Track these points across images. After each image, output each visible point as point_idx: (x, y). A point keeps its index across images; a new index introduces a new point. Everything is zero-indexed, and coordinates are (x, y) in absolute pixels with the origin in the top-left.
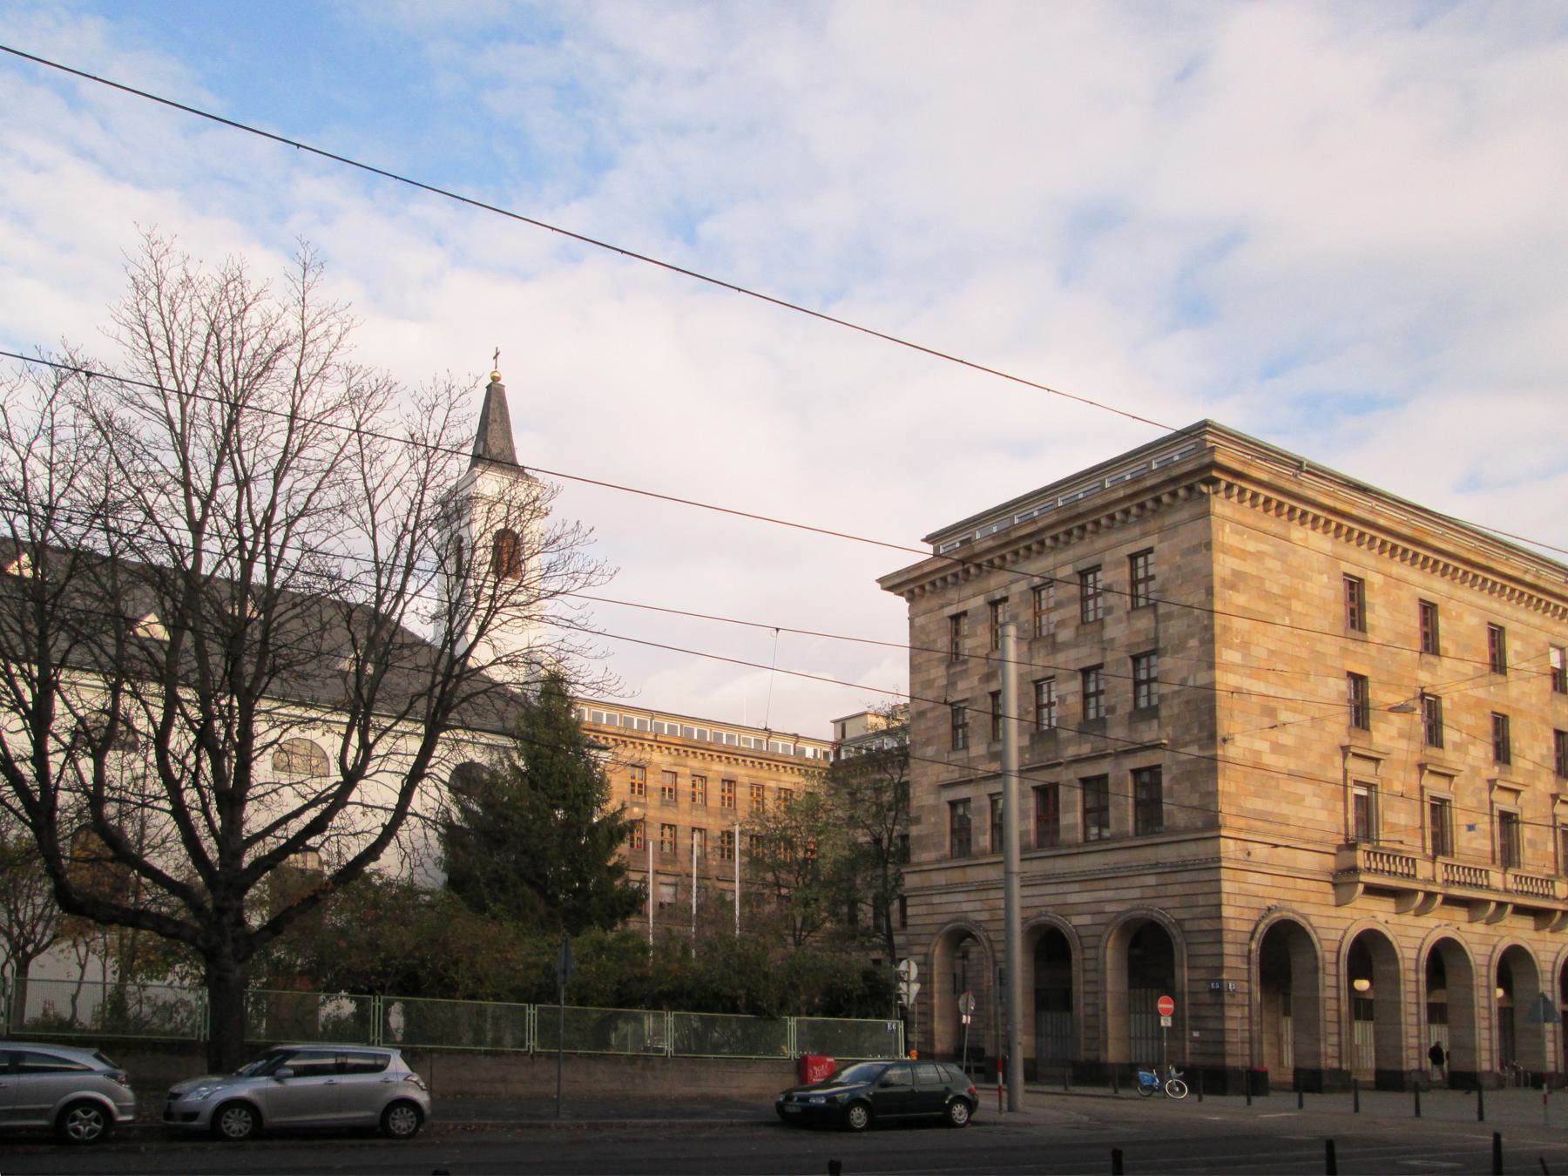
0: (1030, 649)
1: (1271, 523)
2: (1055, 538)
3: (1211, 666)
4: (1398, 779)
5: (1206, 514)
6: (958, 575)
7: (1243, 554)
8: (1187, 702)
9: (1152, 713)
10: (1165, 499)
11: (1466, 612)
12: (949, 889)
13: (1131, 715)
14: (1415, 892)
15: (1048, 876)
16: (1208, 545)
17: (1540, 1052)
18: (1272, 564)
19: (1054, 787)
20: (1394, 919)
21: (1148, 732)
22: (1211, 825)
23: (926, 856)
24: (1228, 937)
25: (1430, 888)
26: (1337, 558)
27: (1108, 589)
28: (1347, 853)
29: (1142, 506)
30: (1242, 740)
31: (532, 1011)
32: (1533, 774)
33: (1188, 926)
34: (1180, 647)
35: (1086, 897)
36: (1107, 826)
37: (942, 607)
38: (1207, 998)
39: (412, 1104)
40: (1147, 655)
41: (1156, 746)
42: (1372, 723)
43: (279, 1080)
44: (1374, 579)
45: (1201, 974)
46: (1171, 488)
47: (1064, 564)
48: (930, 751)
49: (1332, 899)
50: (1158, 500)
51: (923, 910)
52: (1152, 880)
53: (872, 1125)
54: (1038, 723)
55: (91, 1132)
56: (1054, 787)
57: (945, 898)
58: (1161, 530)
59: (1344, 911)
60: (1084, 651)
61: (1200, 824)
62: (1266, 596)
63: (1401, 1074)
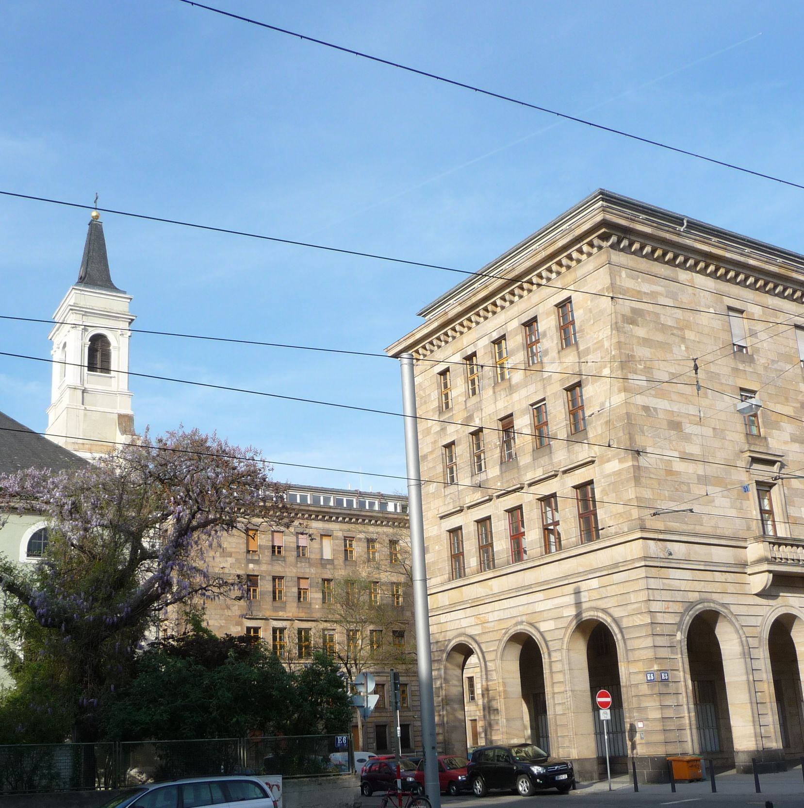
8: (608, 422)
35: (549, 604)
56: (520, 507)
60: (532, 388)
62: (664, 328)
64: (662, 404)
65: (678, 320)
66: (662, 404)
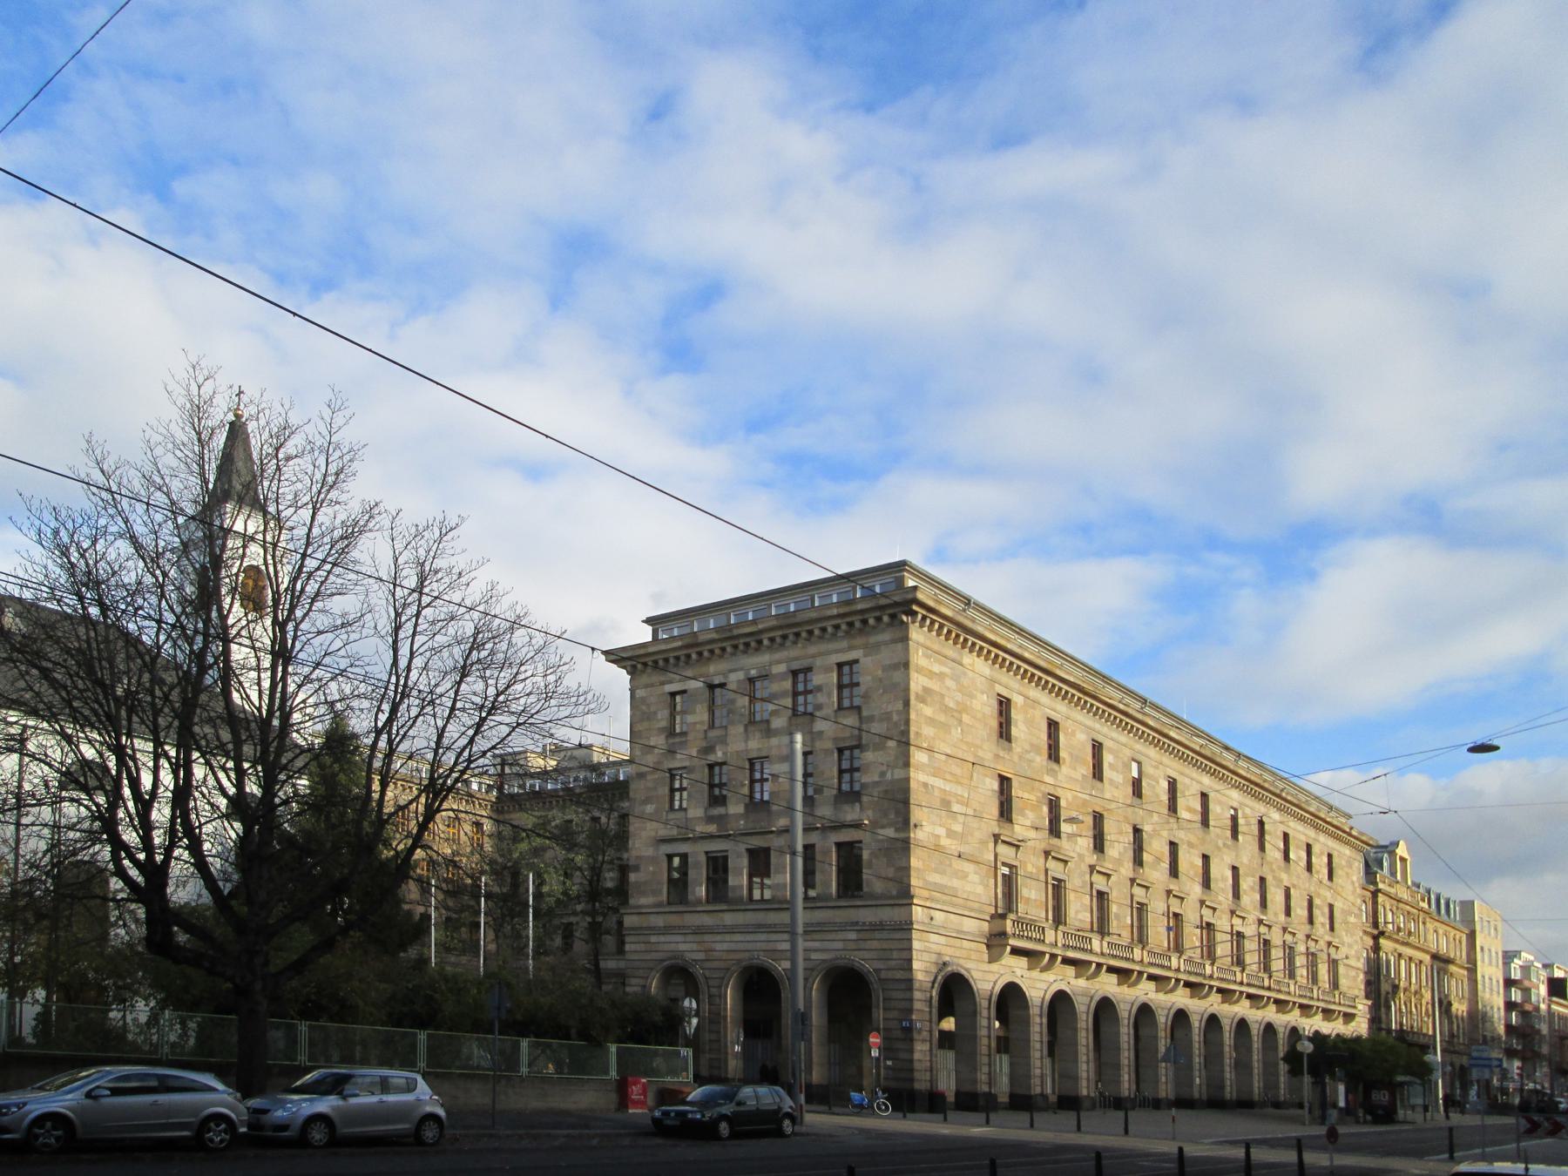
0: (746, 730)
1: (950, 650)
2: (772, 640)
3: (907, 765)
4: (1031, 864)
5: (905, 639)
6: (675, 656)
7: (931, 675)
9: (853, 796)
10: (871, 621)
11: (1079, 728)
12: (667, 930)
13: (836, 797)
14: (1043, 953)
15: (760, 926)
16: (906, 665)
17: (1118, 1082)
18: (950, 683)
19: (767, 851)
20: (1027, 974)
21: (851, 814)
22: (904, 896)
23: (643, 901)
24: (916, 985)
25: (1055, 951)
26: (993, 681)
27: (819, 689)
28: (998, 921)
29: (851, 624)
30: (927, 827)
31: (422, 1036)
32: (1119, 862)
33: (883, 975)
34: (880, 747)
36: (813, 887)
37: (663, 683)
38: (898, 1034)
39: (433, 1117)
40: (851, 748)
41: (857, 825)
42: (1014, 816)
43: (344, 1098)
44: (1017, 700)
45: (894, 1014)
46: (877, 614)
47: (779, 662)
48: (649, 808)
49: (986, 957)
50: (865, 622)
51: (642, 947)
52: (853, 936)
53: (734, 1135)
54: (751, 796)
55: (222, 1141)
56: (767, 851)
57: (662, 939)
58: (865, 647)
59: (995, 967)
61: (894, 893)
62: (946, 709)
63: (1030, 1097)
64: (937, 782)
65: (958, 703)
66: (937, 782)
